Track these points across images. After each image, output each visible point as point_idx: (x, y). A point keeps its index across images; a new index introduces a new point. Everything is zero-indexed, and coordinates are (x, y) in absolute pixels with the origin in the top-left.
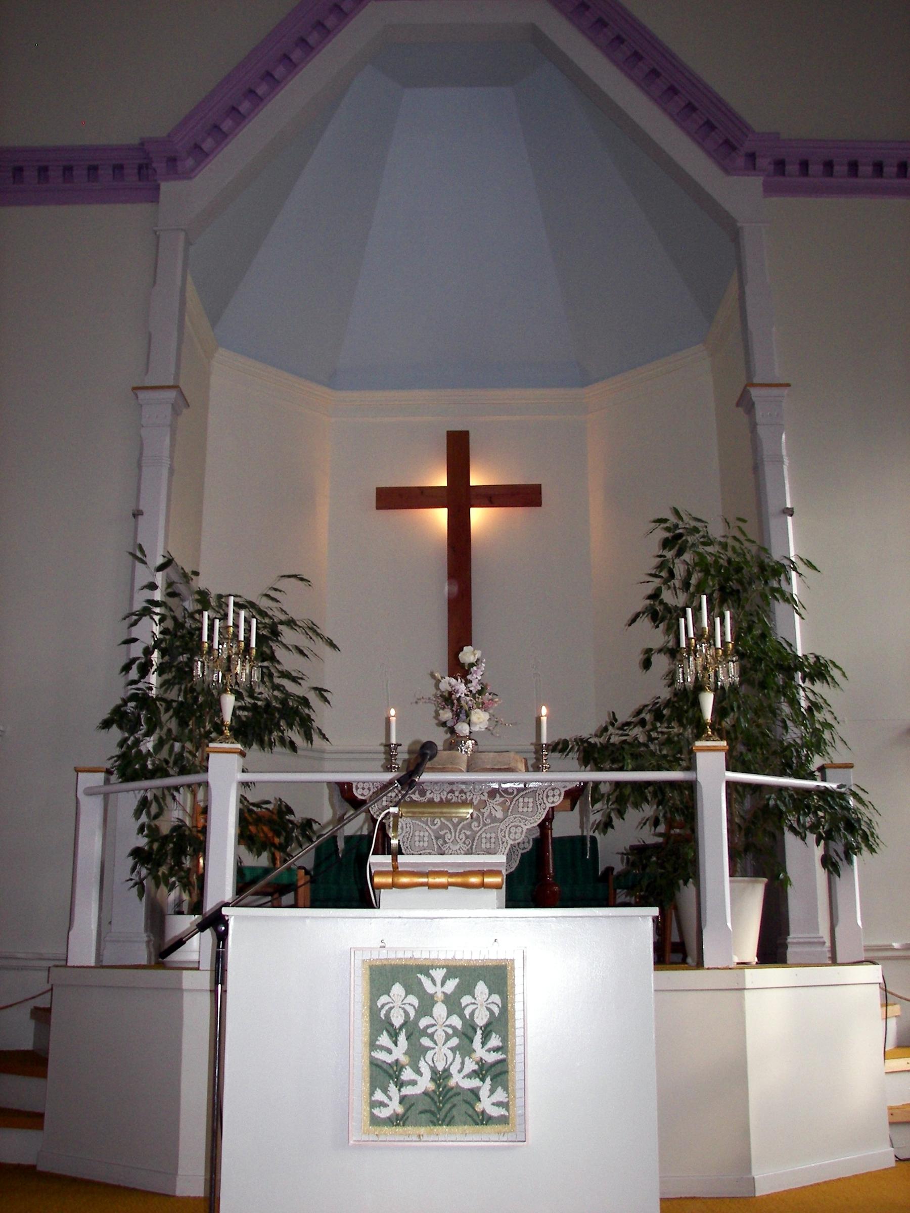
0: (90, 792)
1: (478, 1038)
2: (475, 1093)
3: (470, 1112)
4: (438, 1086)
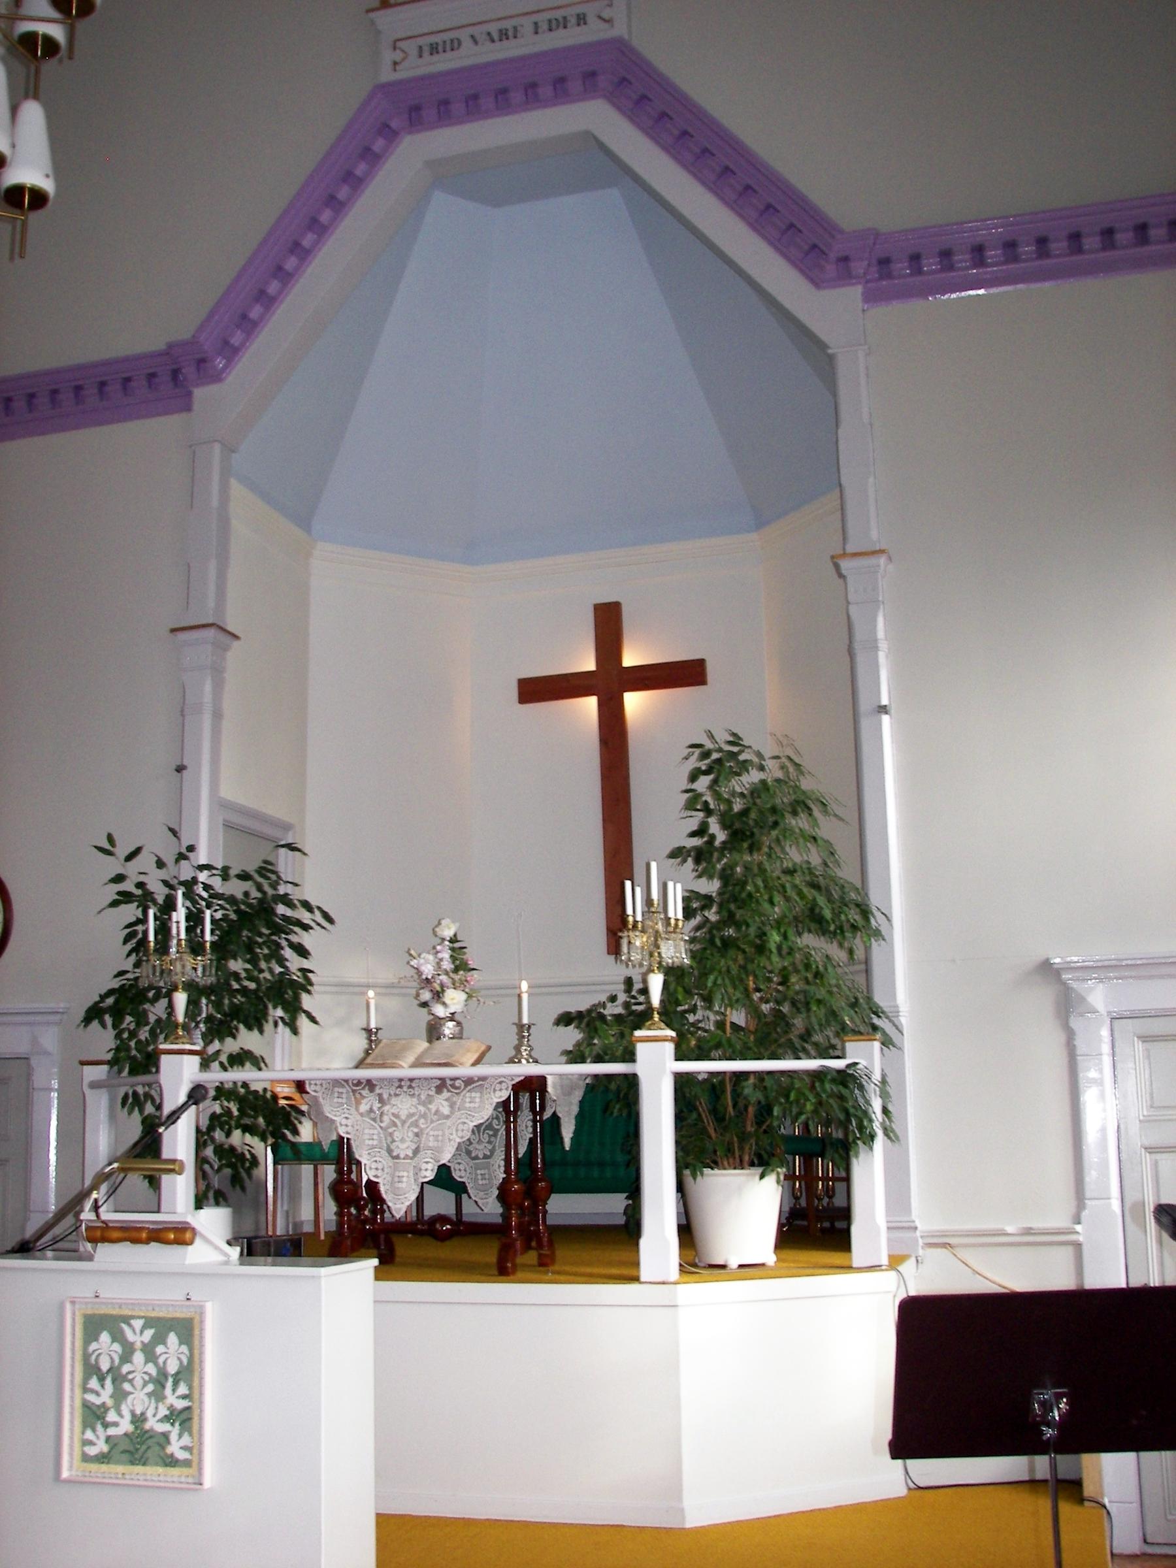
0: (94, 1085)
1: (169, 1384)
2: (166, 1436)
3: (162, 1454)
4: (136, 1428)
